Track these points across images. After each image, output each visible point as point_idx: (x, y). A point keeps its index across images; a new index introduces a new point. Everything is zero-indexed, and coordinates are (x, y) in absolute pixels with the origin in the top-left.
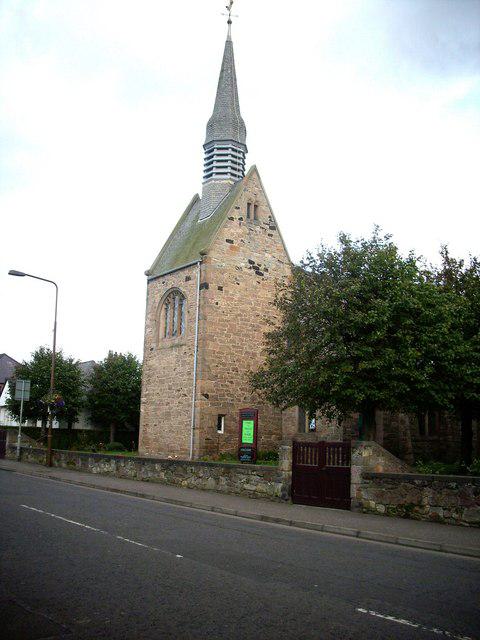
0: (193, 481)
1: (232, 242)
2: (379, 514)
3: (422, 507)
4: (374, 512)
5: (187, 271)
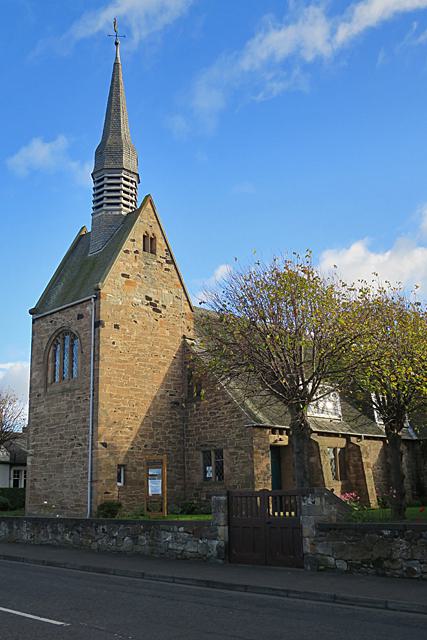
0: (103, 542)
1: (128, 277)
2: (342, 572)
3: (394, 561)
4: (321, 568)
5: (78, 308)
